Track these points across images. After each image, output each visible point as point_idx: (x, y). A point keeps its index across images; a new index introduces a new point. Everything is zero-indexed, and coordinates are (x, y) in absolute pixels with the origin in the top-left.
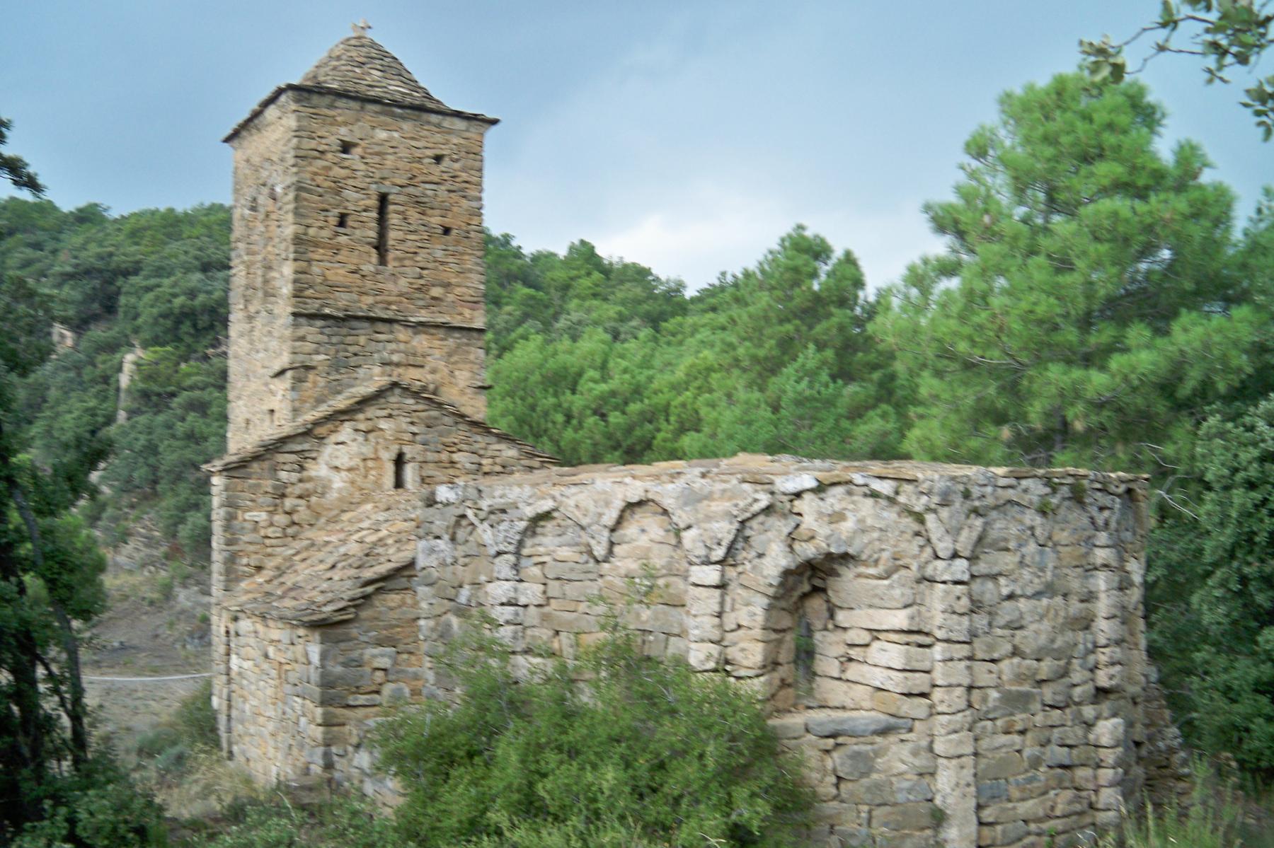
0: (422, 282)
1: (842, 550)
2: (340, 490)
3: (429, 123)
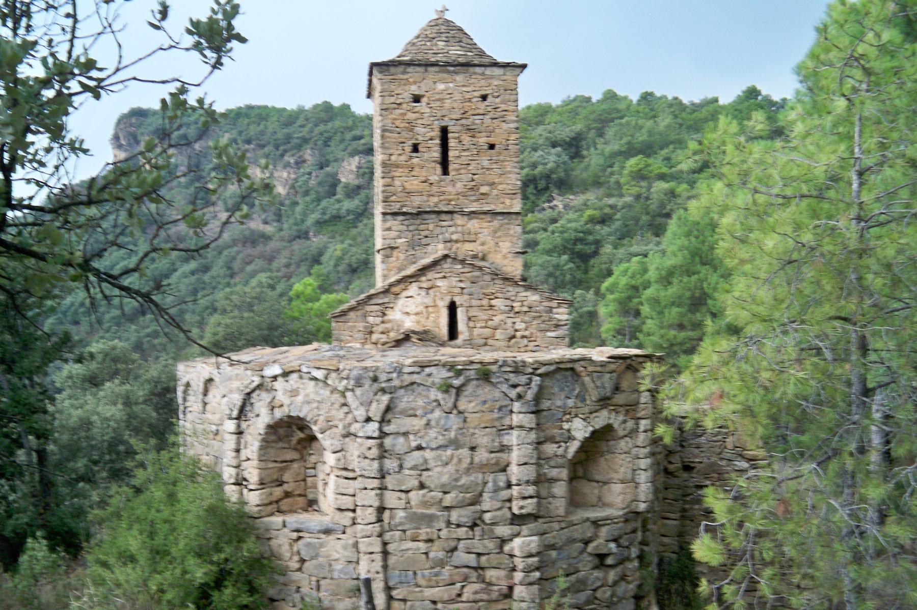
3: (475, 73)
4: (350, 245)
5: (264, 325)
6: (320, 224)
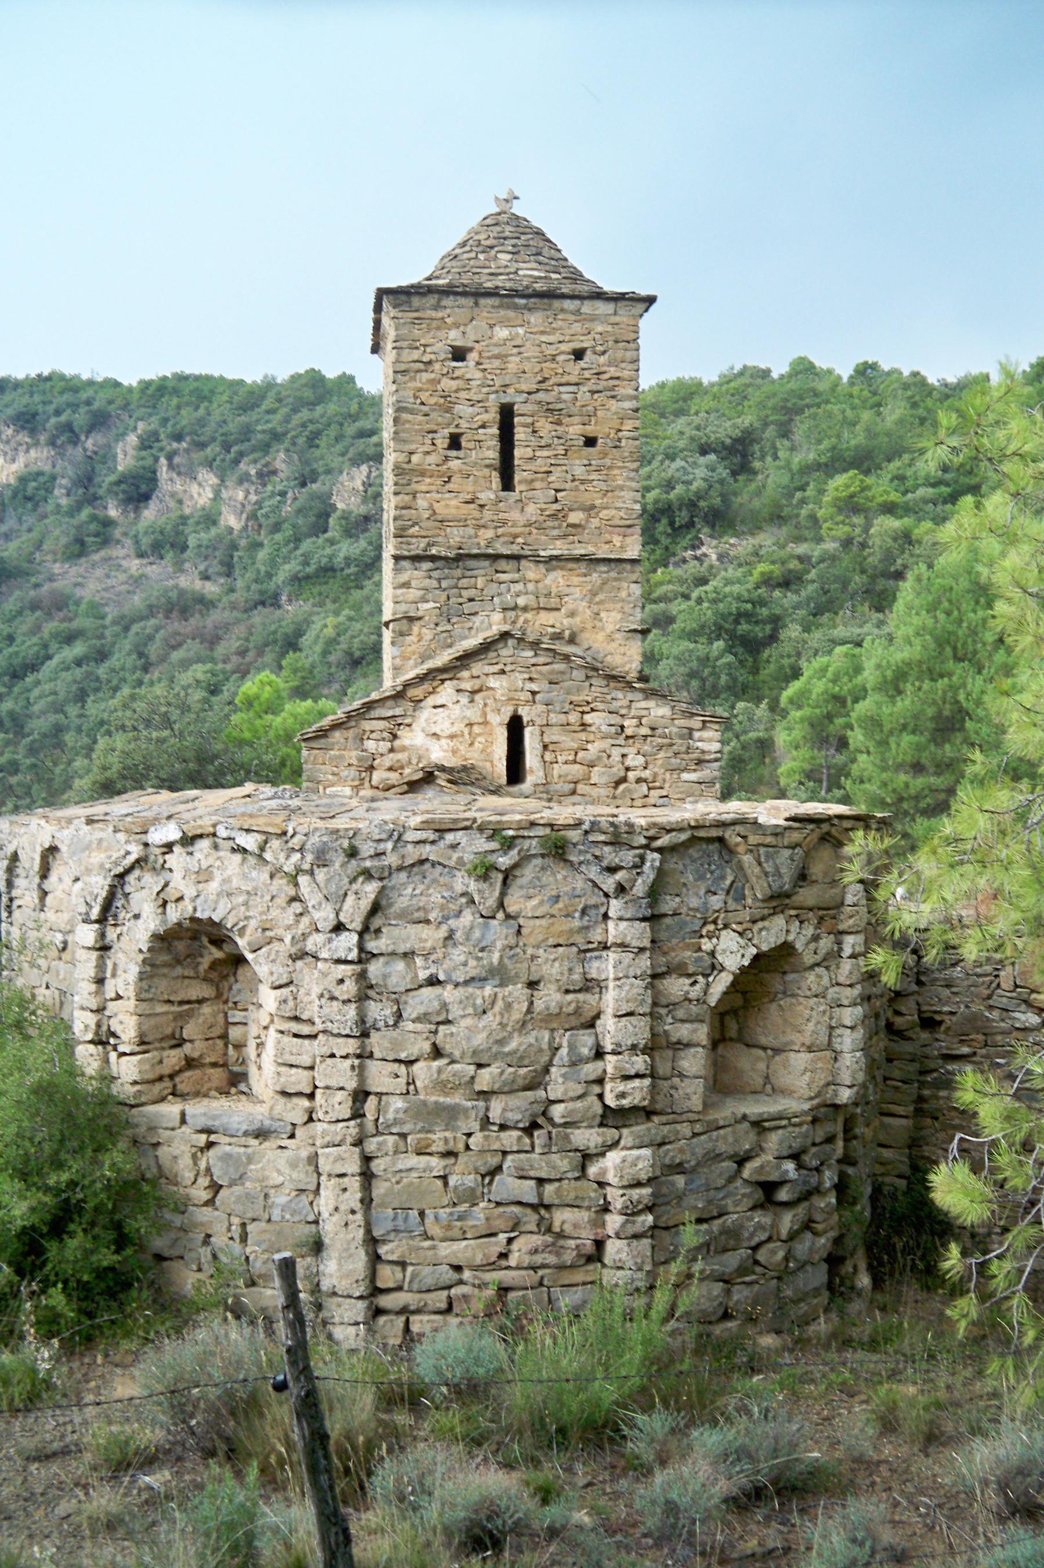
0: (556, 506)
4: (350, 619)
5: (190, 755)
6: (298, 581)
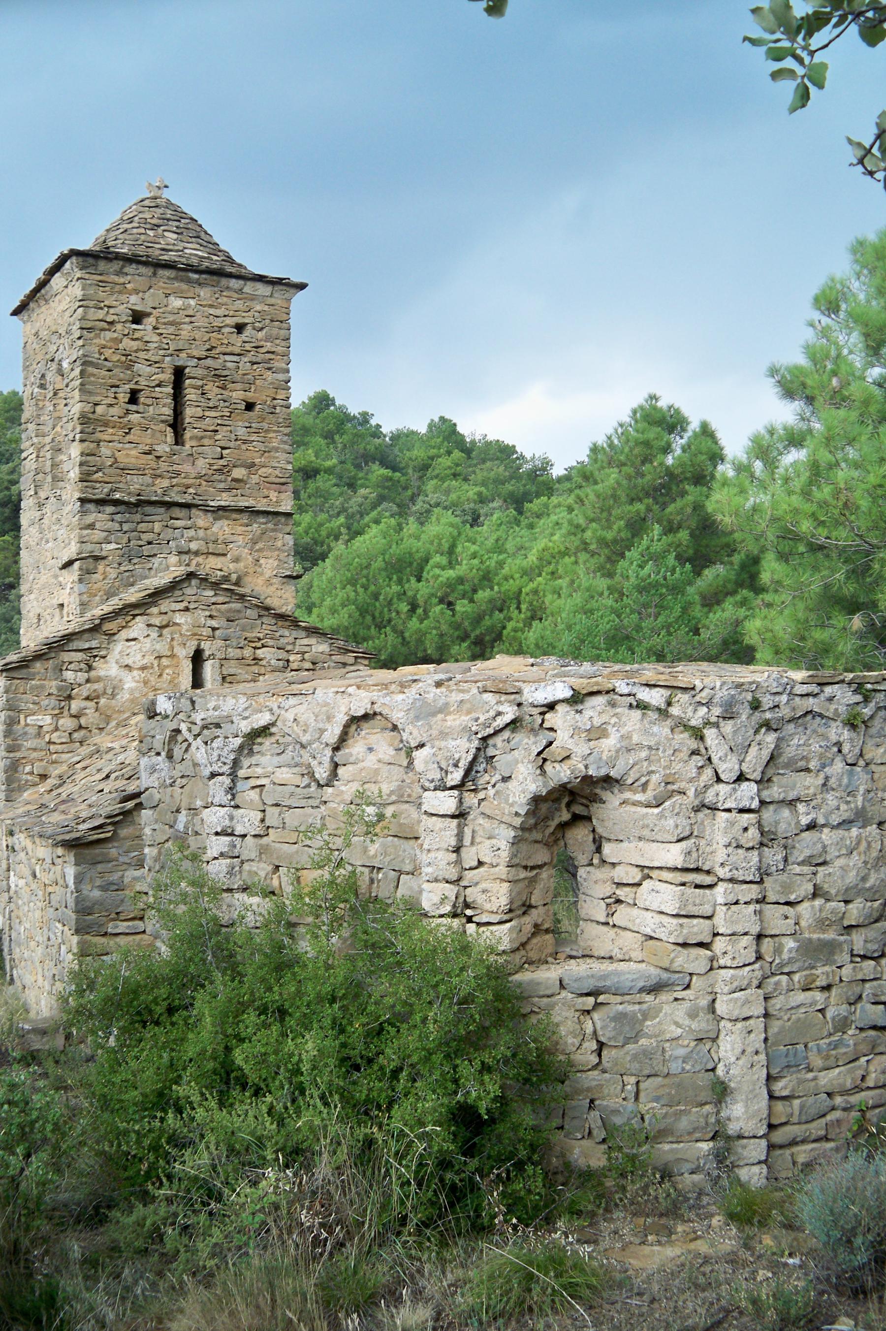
0: (222, 462)
1: (603, 772)
2: (132, 691)
